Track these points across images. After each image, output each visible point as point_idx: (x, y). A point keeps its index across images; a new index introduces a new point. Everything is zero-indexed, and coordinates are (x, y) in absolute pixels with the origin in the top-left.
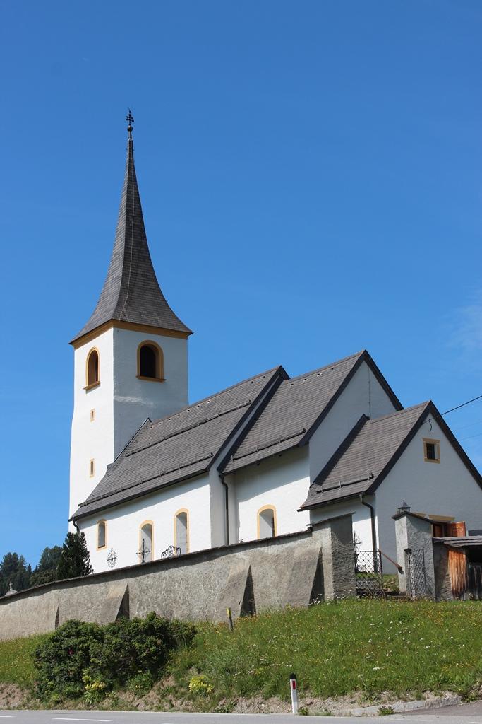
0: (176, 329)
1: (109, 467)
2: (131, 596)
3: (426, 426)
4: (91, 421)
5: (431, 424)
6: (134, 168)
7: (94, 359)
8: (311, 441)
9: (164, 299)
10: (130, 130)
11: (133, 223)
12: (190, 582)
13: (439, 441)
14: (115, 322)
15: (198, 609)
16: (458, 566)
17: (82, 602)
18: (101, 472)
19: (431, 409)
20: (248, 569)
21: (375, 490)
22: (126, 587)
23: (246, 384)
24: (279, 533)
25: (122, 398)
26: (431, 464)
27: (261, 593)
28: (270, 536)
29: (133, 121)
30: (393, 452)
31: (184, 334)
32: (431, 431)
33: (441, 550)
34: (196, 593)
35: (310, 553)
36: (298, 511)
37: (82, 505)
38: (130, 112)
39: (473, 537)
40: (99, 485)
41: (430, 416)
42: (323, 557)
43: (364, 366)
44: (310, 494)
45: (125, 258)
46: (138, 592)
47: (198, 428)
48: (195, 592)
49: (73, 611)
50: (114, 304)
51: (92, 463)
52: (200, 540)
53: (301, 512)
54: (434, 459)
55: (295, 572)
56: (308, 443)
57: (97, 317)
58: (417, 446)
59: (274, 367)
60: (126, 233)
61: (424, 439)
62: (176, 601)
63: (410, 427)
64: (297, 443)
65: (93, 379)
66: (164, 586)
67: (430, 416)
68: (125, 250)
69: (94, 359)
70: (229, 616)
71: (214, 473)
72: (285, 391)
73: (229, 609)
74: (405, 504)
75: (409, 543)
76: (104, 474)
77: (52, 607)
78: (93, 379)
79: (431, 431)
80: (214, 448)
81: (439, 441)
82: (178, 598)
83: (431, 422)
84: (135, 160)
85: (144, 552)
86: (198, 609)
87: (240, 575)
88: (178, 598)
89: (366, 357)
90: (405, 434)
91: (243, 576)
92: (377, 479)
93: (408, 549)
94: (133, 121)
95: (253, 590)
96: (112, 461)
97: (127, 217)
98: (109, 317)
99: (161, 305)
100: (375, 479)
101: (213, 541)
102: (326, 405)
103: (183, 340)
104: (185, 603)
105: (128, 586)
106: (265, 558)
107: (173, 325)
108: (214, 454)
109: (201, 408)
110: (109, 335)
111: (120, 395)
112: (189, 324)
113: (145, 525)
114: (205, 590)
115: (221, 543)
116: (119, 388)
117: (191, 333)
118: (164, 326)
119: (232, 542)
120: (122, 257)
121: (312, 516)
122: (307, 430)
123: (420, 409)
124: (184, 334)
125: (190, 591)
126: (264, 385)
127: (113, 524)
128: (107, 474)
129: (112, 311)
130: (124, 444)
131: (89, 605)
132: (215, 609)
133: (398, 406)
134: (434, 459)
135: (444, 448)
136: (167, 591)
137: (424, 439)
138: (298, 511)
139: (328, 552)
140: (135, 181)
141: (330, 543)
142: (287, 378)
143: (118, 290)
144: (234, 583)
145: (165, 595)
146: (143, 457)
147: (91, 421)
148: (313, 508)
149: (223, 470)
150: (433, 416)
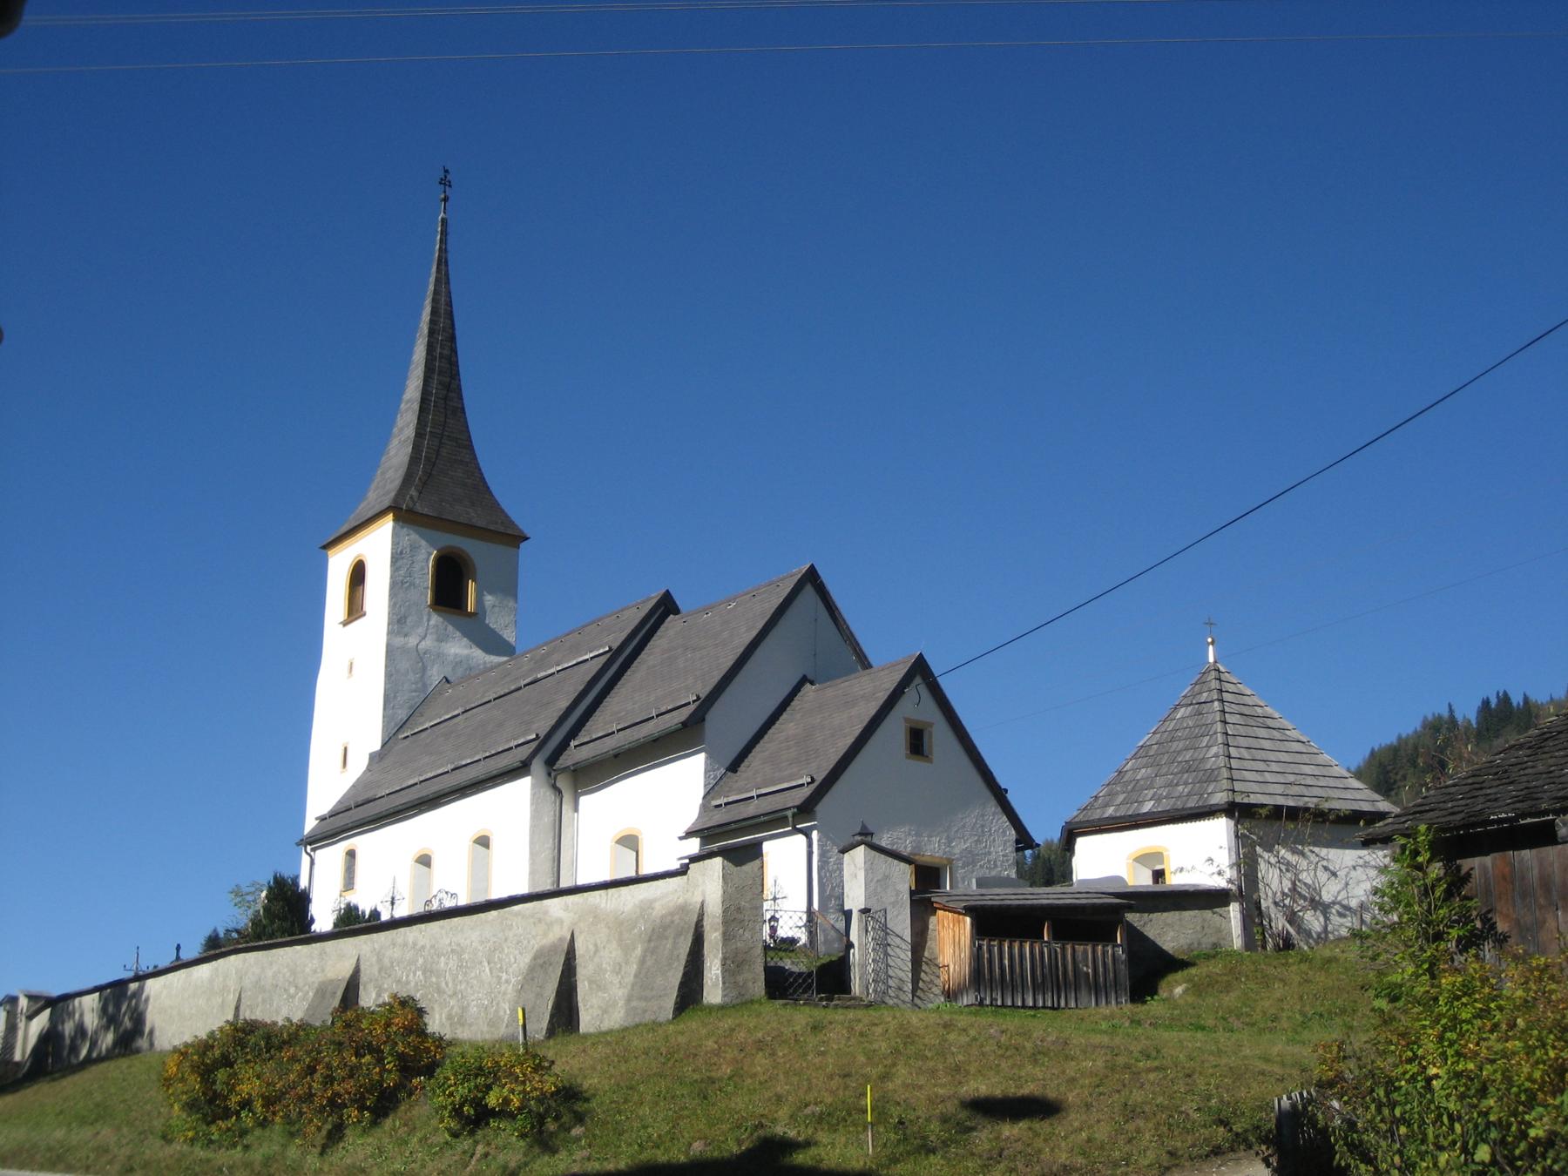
0: (502, 529)
1: (373, 757)
2: (363, 978)
3: (910, 692)
4: (349, 677)
5: (917, 694)
6: (446, 262)
7: (358, 574)
8: (708, 717)
9: (484, 478)
10: (446, 200)
11: (438, 350)
12: (466, 956)
13: (931, 725)
14: (405, 514)
15: (477, 1006)
16: (956, 943)
17: (280, 984)
18: (358, 765)
19: (920, 669)
20: (569, 937)
21: (816, 805)
22: (354, 961)
23: (606, 621)
24: (646, 870)
25: (399, 641)
26: (916, 765)
27: (590, 982)
28: (633, 874)
29: (450, 186)
30: (850, 740)
31: (515, 538)
32: (917, 707)
33: (923, 903)
34: (476, 977)
35: (683, 909)
36: (681, 838)
37: (322, 819)
38: (446, 171)
39: (983, 891)
40: (353, 786)
41: (918, 680)
42: (705, 918)
43: (809, 590)
44: (705, 807)
45: (420, 407)
46: (375, 970)
47: (521, 692)
48: (473, 975)
49: (264, 1001)
50: (397, 483)
51: (346, 749)
52: (510, 880)
53: (684, 841)
54: (923, 755)
55: (652, 944)
56: (704, 720)
57: (369, 504)
58: (894, 732)
59: (656, 595)
60: (426, 366)
61: (907, 720)
62: (439, 991)
63: (882, 696)
64: (683, 718)
65: (355, 609)
66: (421, 961)
67: (918, 680)
68: (422, 393)
69: (358, 574)
70: (521, 1022)
71: (538, 765)
72: (671, 632)
73: (524, 1010)
74: (864, 826)
75: (867, 898)
76: (364, 769)
77: (229, 991)
78: (355, 609)
79: (917, 707)
80: (543, 725)
81: (931, 725)
82: (443, 985)
83: (918, 688)
84: (449, 248)
85: (393, 898)
86: (477, 1006)
87: (553, 949)
88: (443, 985)
89: (811, 576)
90: (872, 709)
91: (711, 955)
92: (821, 783)
93: (865, 909)
94: (450, 186)
95: (575, 975)
96: (377, 746)
97: (429, 342)
98: (387, 503)
99: (479, 489)
100: (816, 784)
101: (529, 888)
102: (738, 655)
103: (516, 549)
104: (455, 994)
105: (358, 960)
106: (595, 915)
107: (496, 523)
108: (542, 736)
109: (531, 659)
110: (385, 528)
111: (399, 633)
112: (523, 523)
113: (421, 856)
114: (491, 970)
115: (547, 886)
116: (398, 622)
117: (527, 539)
118: (481, 523)
119: (564, 884)
120: (416, 406)
121: (702, 844)
122: (703, 696)
123: (901, 666)
124: (515, 538)
125: (465, 974)
126: (636, 622)
127: (367, 844)
128: (369, 769)
129: (393, 494)
130: (402, 714)
131: (292, 990)
132: (507, 1007)
133: (865, 664)
134: (923, 755)
135: (940, 738)
136: (424, 973)
137: (907, 720)
138: (681, 838)
139: (714, 907)
140: (448, 282)
141: (720, 893)
142: (676, 611)
143: (406, 459)
144: (540, 962)
145: (421, 977)
146: (428, 741)
147: (349, 677)
148: (704, 833)
149: (555, 764)
150: (924, 679)
